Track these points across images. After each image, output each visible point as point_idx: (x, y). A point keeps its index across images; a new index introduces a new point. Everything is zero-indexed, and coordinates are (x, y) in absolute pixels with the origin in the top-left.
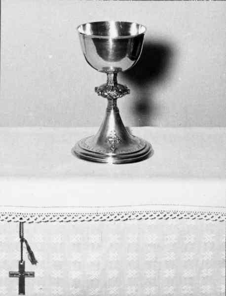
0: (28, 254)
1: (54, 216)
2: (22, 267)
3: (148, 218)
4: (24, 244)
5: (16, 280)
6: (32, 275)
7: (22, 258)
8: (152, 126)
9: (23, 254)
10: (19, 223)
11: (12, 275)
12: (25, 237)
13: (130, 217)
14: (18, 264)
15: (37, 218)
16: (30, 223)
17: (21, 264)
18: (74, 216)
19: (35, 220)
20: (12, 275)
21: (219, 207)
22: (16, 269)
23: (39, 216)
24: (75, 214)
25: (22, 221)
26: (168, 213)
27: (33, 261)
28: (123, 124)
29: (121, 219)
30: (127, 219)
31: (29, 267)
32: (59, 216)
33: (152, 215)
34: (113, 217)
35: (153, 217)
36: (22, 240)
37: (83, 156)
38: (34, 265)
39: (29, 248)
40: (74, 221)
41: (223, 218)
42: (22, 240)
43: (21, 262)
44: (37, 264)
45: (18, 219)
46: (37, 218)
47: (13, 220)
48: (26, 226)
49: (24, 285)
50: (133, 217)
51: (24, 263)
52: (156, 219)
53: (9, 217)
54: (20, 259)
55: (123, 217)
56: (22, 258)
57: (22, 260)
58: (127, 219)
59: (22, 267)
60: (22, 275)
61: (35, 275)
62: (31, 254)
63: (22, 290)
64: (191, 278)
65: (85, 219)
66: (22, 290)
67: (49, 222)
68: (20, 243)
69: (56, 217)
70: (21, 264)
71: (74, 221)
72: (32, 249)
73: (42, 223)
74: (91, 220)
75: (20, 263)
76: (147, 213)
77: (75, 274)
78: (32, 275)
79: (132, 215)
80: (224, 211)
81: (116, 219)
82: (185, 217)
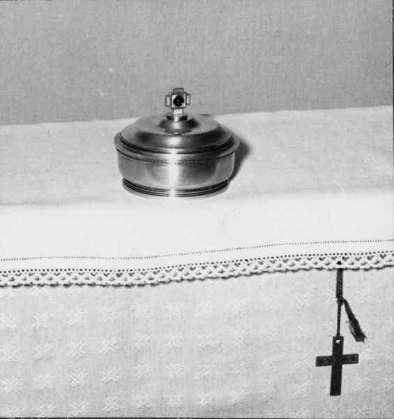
2: (338, 347)
6: (353, 359)
11: (321, 361)
12: (345, 296)
20: (321, 361)
24: (296, 257)
27: (359, 335)
31: (350, 346)
36: (341, 300)
38: (361, 343)
42: (341, 300)
59: (338, 347)
60: (337, 360)
63: (336, 389)
66: (336, 389)
68: (337, 305)
70: (338, 341)
78: (353, 359)
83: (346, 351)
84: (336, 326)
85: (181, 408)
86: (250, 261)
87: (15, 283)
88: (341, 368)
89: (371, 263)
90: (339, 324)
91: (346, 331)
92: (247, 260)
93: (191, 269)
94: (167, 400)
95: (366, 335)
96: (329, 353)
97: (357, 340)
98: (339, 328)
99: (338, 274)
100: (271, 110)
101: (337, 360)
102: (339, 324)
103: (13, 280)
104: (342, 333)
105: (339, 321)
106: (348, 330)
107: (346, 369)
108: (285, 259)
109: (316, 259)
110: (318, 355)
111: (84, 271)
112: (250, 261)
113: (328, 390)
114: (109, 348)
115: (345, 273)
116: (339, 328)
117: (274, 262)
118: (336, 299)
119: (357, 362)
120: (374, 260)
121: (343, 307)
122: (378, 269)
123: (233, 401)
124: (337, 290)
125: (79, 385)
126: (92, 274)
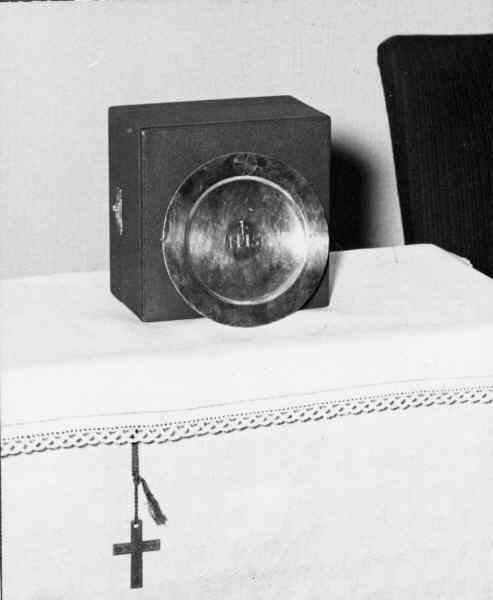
0: (146, 500)
1: (205, 424)
2: (136, 533)
3: (478, 401)
6: (155, 545)
7: (136, 513)
8: (378, 246)
10: (129, 447)
11: (118, 550)
12: (142, 474)
13: (342, 409)
14: (129, 526)
16: (121, 444)
17: (136, 526)
18: (147, 432)
19: (402, 403)
20: (118, 550)
22: (127, 539)
23: (178, 428)
25: (135, 441)
27: (159, 518)
28: (439, 245)
29: (389, 407)
31: (150, 532)
33: (380, 404)
34: (286, 416)
35: (382, 407)
36: (138, 479)
39: (149, 495)
41: (491, 396)
42: (138, 479)
43: (136, 523)
44: (167, 522)
45: (125, 437)
47: (158, 440)
48: (141, 447)
49: (141, 567)
50: (397, 403)
52: (325, 418)
54: (132, 518)
55: (328, 412)
56: (136, 513)
57: (136, 517)
59: (136, 533)
60: (137, 548)
63: (137, 581)
64: (207, 580)
65: (115, 440)
66: (137, 581)
70: (136, 526)
72: (156, 496)
73: (62, 450)
74: (111, 443)
78: (155, 545)
79: (122, 434)
82: (379, 408)
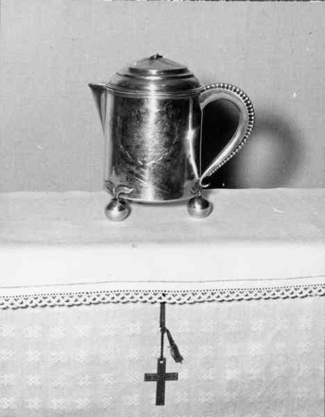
1: (213, 294)
2: (161, 367)
4: (165, 335)
5: (153, 384)
6: (174, 377)
9: (164, 350)
10: (158, 306)
11: (148, 378)
12: (167, 326)
15: (190, 298)
19: (188, 299)
20: (148, 378)
21: (246, 280)
24: (126, 292)
26: (305, 289)
27: (178, 358)
30: (306, 296)
31: (171, 367)
32: (248, 293)
36: (164, 330)
37: (133, 197)
38: (179, 363)
40: (220, 301)
42: (164, 330)
46: (190, 298)
50: (315, 292)
51: (165, 363)
53: (43, 300)
58: (306, 296)
59: (161, 367)
60: (161, 377)
61: (179, 376)
62: (174, 348)
63: (160, 400)
66: (160, 400)
67: (29, 308)
68: (160, 333)
69: (82, 299)
70: (161, 362)
71: (220, 301)
75: (159, 361)
76: (296, 289)
77: (231, 374)
78: (174, 377)
80: (321, 281)
81: (283, 296)
83: (168, 371)
84: (160, 351)
85: (37, 411)
86: (90, 294)
87: (266, 297)
88: (164, 383)
89: (184, 299)
90: (162, 349)
91: (168, 354)
92: (87, 293)
93: (203, 294)
94: (28, 403)
95: (184, 358)
96: (155, 371)
97: (177, 362)
98: (162, 351)
99: (161, 306)
100: (90, 191)
101: (161, 377)
102: (162, 349)
103: (265, 294)
104: (164, 356)
105: (162, 345)
106: (169, 352)
107: (169, 384)
108: (118, 293)
109: (141, 294)
110: (146, 372)
111: (110, 292)
112: (90, 294)
113: (154, 401)
114: (109, 381)
115: (166, 304)
116: (162, 351)
117: (108, 295)
118: (160, 329)
119: (177, 379)
120: (187, 297)
121: (165, 335)
122: (104, 303)
123: (79, 407)
124: (161, 321)
125: (34, 409)
126: (15, 300)
